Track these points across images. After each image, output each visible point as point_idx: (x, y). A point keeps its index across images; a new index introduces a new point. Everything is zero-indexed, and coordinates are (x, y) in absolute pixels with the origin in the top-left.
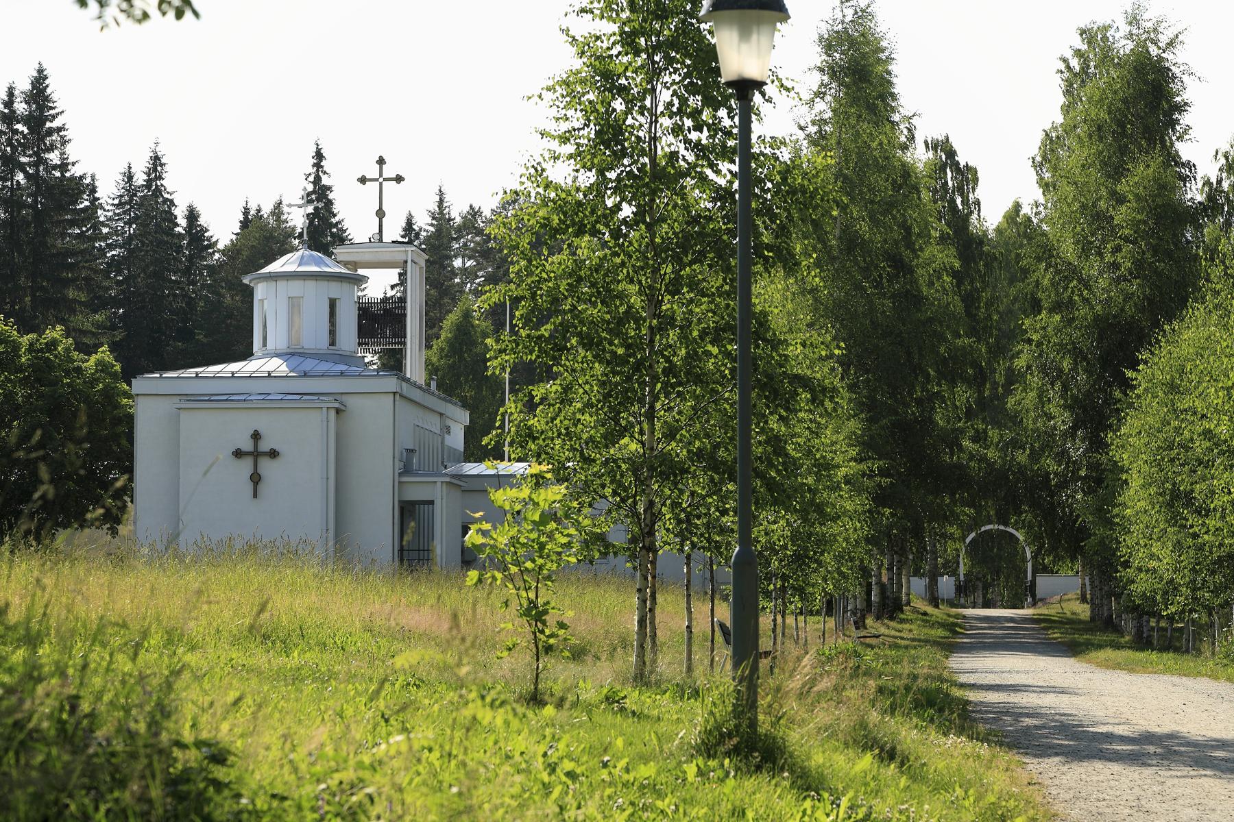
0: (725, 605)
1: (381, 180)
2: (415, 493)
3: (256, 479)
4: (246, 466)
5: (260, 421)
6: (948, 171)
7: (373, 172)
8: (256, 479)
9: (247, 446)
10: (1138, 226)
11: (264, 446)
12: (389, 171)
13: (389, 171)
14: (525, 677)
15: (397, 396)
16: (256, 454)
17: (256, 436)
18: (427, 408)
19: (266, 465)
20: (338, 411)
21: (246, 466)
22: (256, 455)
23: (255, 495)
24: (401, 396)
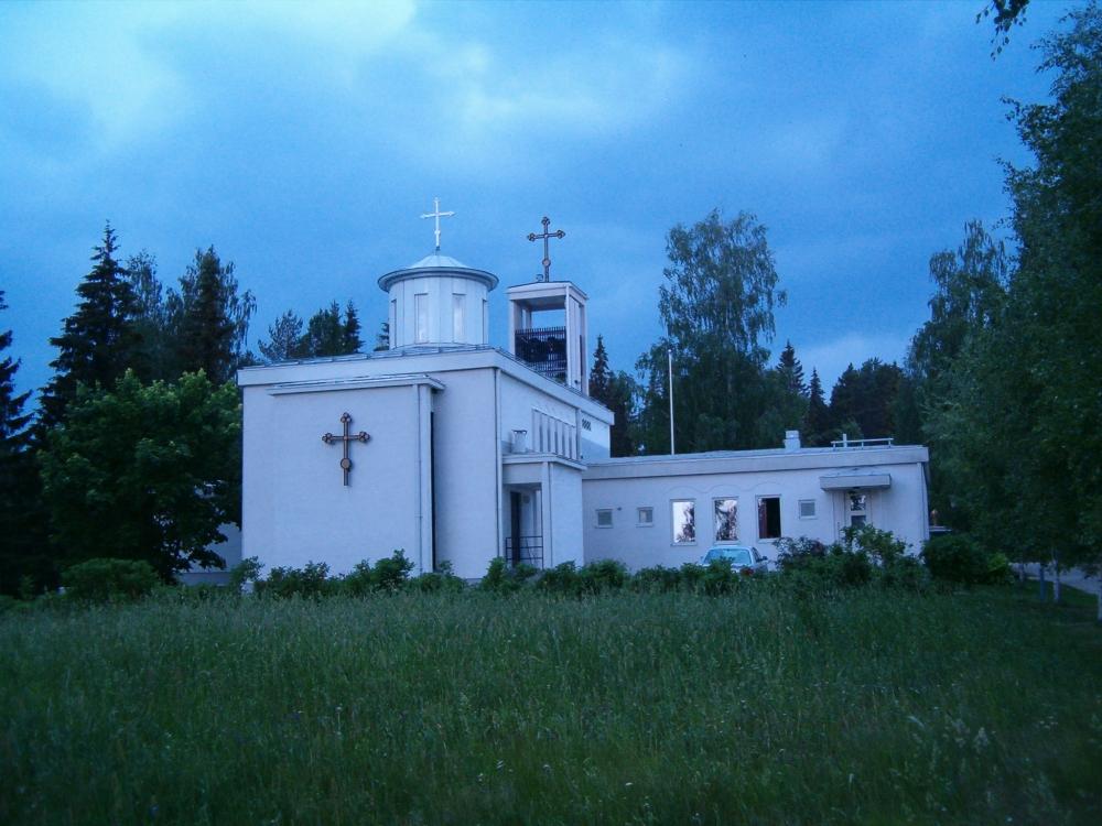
0: (527, 446)
1: (546, 236)
2: (520, 477)
3: (348, 468)
4: (338, 451)
5: (352, 404)
6: (964, 760)
7: (540, 230)
8: (348, 468)
9: (338, 431)
10: (1069, 52)
11: (338, 431)
12: (552, 229)
13: (552, 229)
14: (824, 633)
15: (499, 373)
16: (348, 439)
17: (347, 420)
18: (565, 403)
19: (358, 450)
20: (435, 391)
21: (338, 451)
22: (348, 440)
23: (347, 482)
24: (504, 373)
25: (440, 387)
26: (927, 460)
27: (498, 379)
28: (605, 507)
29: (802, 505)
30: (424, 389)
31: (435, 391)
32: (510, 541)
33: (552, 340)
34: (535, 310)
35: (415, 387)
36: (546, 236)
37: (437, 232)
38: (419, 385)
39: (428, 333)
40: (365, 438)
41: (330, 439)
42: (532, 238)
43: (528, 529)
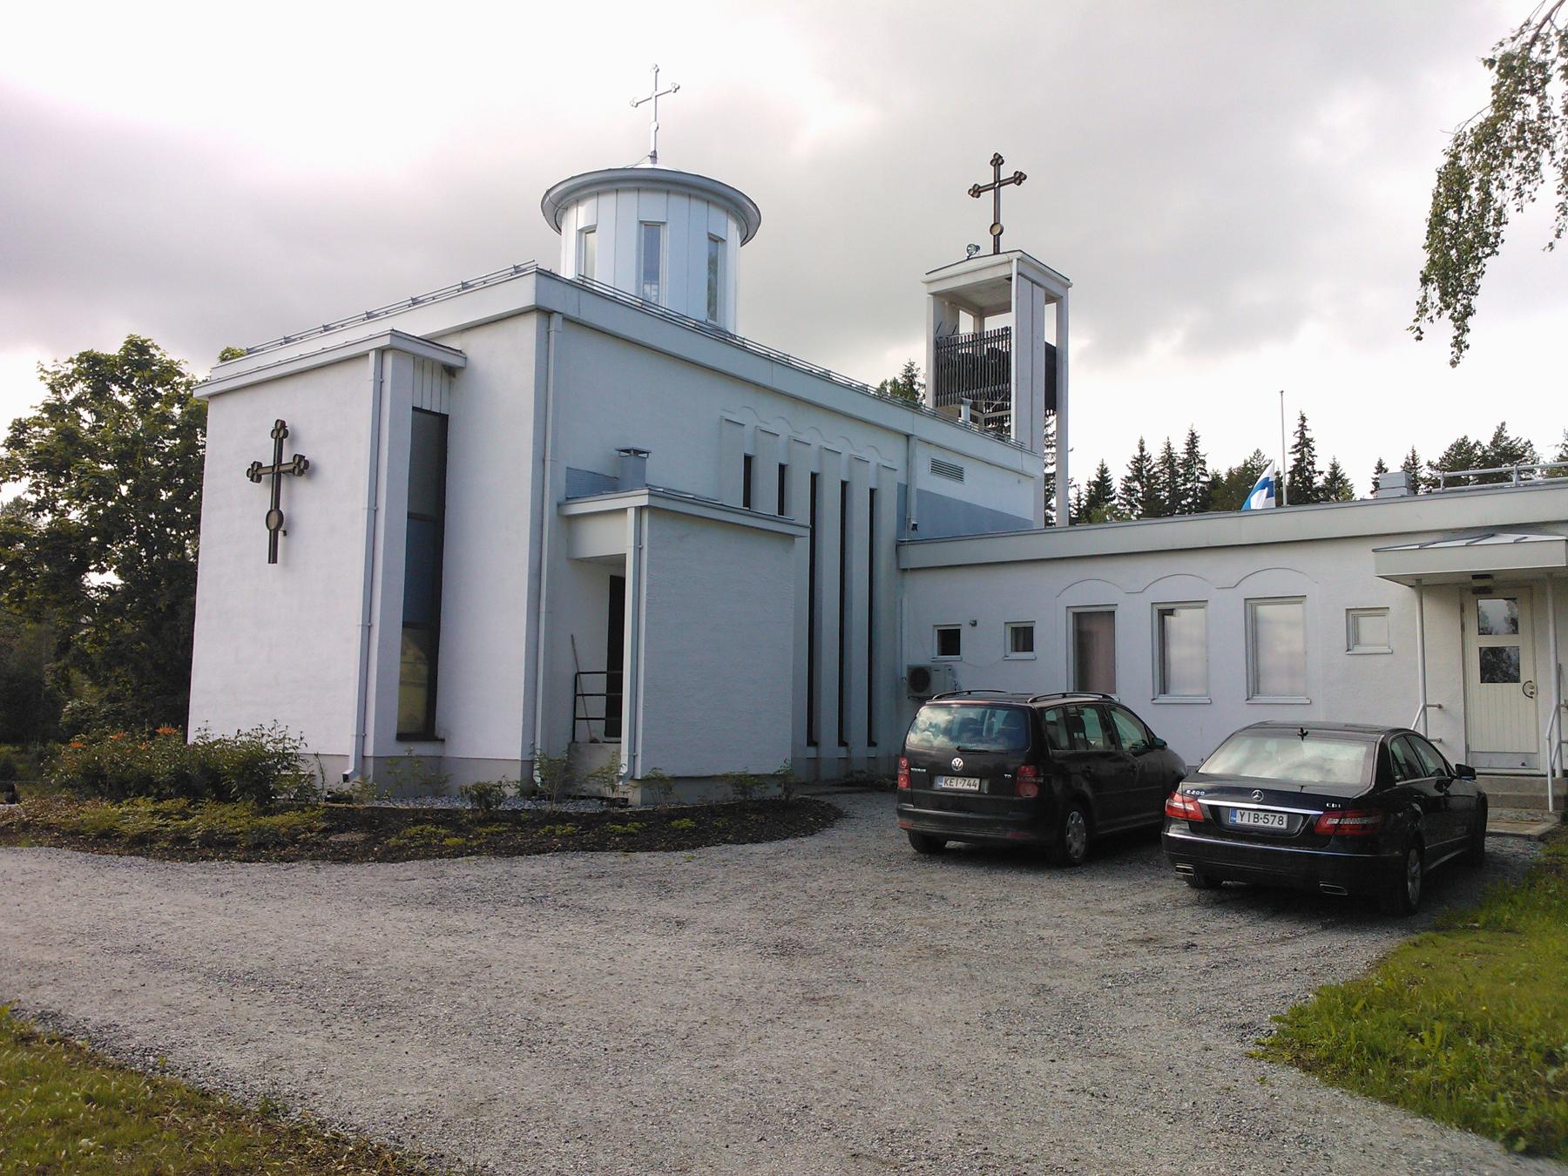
1: (998, 184)
12: (1006, 172)
13: (1006, 172)
15: (556, 321)
17: (281, 432)
28: (948, 621)
31: (451, 371)
36: (998, 184)
38: (382, 351)
40: (302, 467)
42: (976, 191)
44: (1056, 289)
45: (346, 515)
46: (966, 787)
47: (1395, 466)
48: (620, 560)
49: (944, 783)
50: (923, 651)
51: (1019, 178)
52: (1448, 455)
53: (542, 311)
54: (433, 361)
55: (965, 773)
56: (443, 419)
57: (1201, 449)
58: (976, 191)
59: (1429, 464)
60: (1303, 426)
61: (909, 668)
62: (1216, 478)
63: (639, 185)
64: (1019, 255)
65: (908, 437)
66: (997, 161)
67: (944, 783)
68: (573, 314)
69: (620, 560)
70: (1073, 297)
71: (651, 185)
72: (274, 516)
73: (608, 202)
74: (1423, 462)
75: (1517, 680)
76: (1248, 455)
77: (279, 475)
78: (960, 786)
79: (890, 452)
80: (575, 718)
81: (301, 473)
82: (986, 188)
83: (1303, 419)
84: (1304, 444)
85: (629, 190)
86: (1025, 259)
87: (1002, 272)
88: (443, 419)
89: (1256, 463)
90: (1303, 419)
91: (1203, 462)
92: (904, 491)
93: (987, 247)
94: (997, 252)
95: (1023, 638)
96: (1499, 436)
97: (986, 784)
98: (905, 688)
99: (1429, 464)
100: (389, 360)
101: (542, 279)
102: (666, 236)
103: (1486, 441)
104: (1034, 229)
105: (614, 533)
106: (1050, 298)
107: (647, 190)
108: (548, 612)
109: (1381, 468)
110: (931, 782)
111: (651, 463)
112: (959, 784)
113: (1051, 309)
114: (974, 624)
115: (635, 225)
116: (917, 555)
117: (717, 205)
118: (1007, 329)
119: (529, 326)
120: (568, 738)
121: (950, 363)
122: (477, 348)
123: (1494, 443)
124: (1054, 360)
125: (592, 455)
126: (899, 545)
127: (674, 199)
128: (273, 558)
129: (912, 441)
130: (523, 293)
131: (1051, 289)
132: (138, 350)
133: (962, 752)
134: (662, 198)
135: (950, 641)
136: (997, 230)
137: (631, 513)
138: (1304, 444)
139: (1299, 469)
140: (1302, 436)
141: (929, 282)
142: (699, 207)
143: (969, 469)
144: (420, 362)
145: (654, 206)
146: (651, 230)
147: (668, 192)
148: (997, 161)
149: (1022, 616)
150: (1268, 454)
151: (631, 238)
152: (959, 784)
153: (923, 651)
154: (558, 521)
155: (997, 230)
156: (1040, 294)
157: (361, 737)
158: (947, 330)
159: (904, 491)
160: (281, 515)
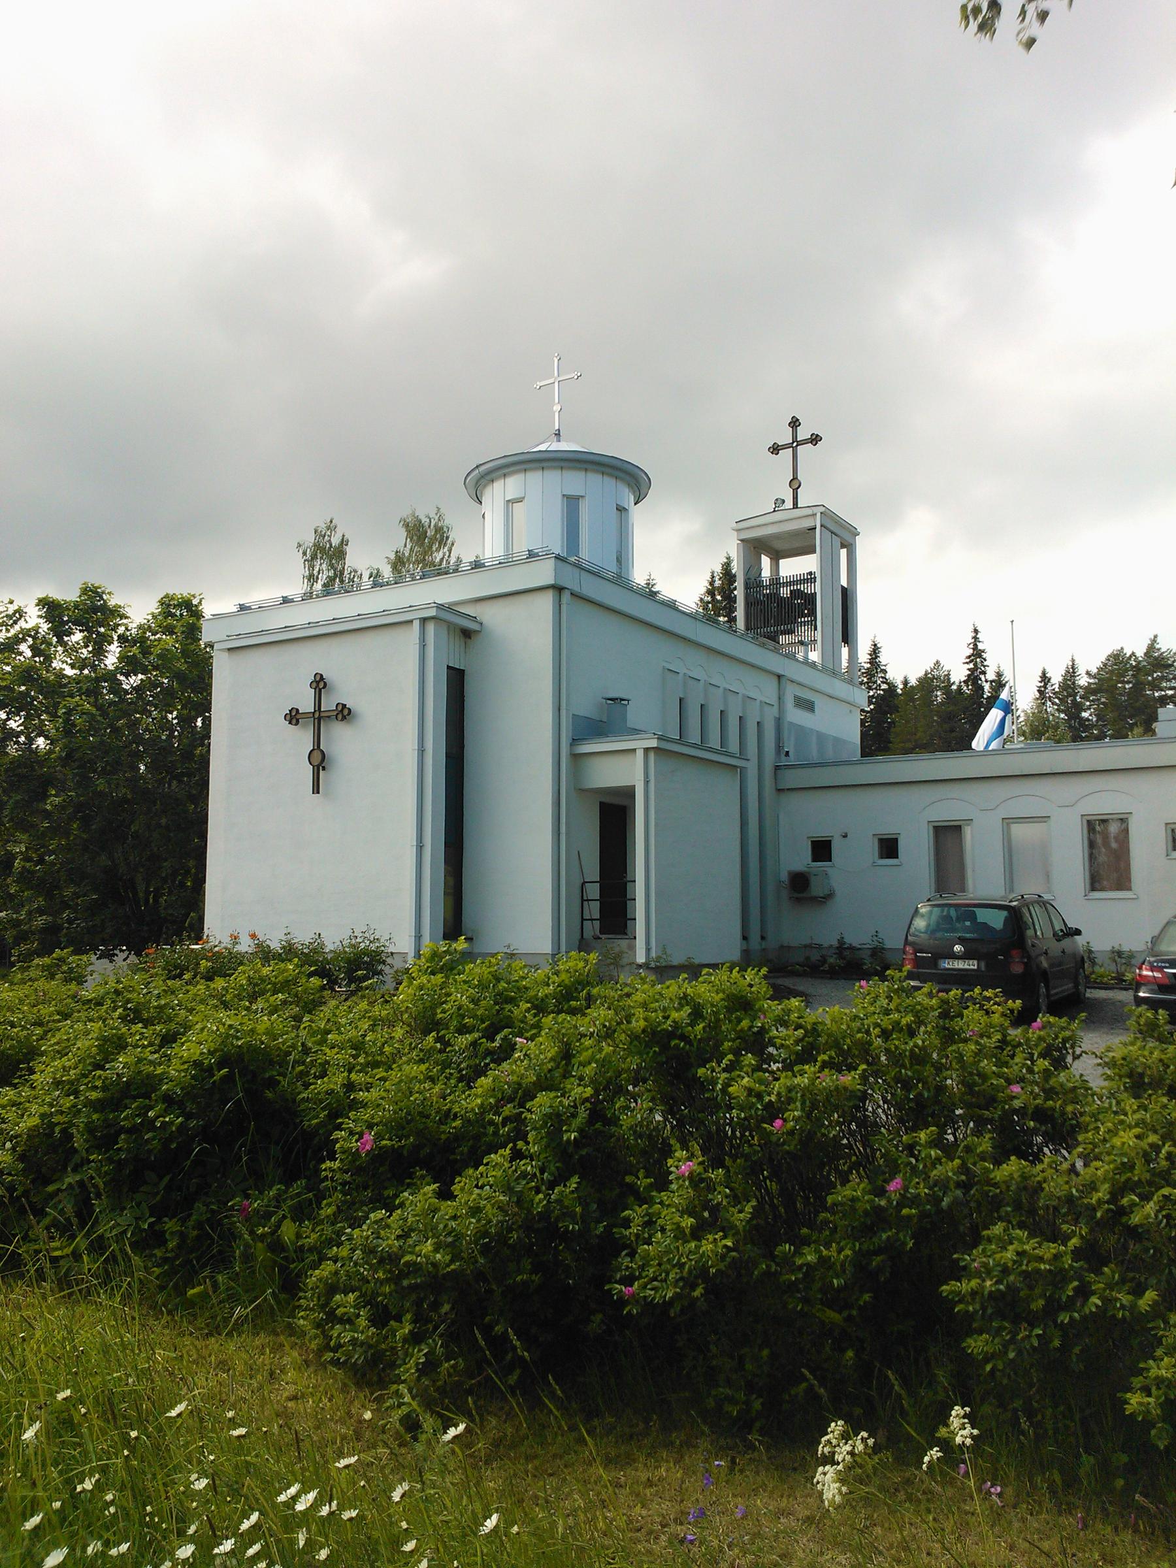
1: (795, 444)
3: (320, 762)
4: (303, 739)
9: (306, 704)
12: (803, 434)
13: (803, 434)
15: (566, 596)
17: (320, 684)
19: (339, 738)
21: (303, 739)
25: (473, 626)
26: (909, 627)
27: (564, 607)
28: (821, 833)
29: (935, 828)
30: (431, 628)
31: (467, 634)
32: (594, 891)
33: (796, 594)
34: (783, 557)
35: (416, 624)
36: (795, 444)
37: (557, 408)
38: (424, 620)
39: (492, 549)
40: (344, 713)
41: (294, 717)
42: (775, 449)
43: (451, 881)
44: (847, 537)
45: (391, 750)
46: (966, 967)
47: (1056, 678)
48: (629, 792)
49: (947, 964)
50: (801, 860)
51: (815, 439)
52: (1105, 665)
53: (558, 589)
54: (455, 625)
55: (964, 957)
56: (461, 673)
57: (883, 659)
58: (775, 449)
59: (1088, 673)
60: (975, 638)
61: (790, 873)
62: (892, 687)
63: (563, 464)
64: (823, 509)
65: (779, 677)
66: (795, 423)
67: (947, 964)
68: (576, 589)
69: (629, 792)
70: (860, 543)
71: (571, 465)
72: (317, 754)
73: (535, 479)
74: (1081, 670)
75: (814, 860)
76: (928, 665)
77: (319, 719)
78: (961, 966)
79: (766, 691)
80: (583, 920)
81: (344, 718)
82: (785, 447)
83: (976, 631)
84: (977, 655)
85: (554, 468)
86: (827, 514)
87: (808, 523)
88: (461, 673)
89: (936, 673)
90: (976, 631)
91: (885, 672)
92: (779, 722)
93: (789, 504)
94: (795, 506)
95: (889, 848)
96: (1151, 648)
97: (983, 964)
98: (785, 894)
99: (1088, 673)
100: (431, 628)
101: (559, 562)
102: (584, 509)
103: (1140, 653)
104: (829, 485)
105: (623, 767)
106: (843, 546)
107: (569, 468)
108: (567, 834)
109: (1045, 678)
110: (936, 966)
111: (631, 709)
112: (960, 965)
113: (844, 552)
114: (845, 836)
115: (560, 496)
116: (792, 779)
117: (622, 480)
118: (810, 573)
119: (546, 602)
120: (578, 936)
121: (758, 602)
122: (492, 616)
123: (1147, 654)
124: (847, 598)
125: (585, 705)
126: (777, 768)
127: (590, 475)
128: (316, 789)
129: (783, 680)
130: (544, 573)
131: (842, 536)
132: (92, 593)
133: (961, 941)
134: (581, 474)
135: (822, 850)
136: (795, 484)
137: (640, 754)
138: (977, 655)
139: (974, 678)
140: (975, 647)
141: (738, 530)
142: (610, 482)
143: (819, 701)
144: (450, 626)
145: (575, 482)
146: (572, 502)
147: (586, 470)
148: (795, 423)
149: (888, 830)
150: (947, 665)
151: (557, 508)
152: (960, 965)
153: (801, 860)
154: (571, 759)
155: (795, 484)
156: (837, 542)
157: (418, 937)
158: (752, 575)
159: (779, 722)
160: (322, 752)
